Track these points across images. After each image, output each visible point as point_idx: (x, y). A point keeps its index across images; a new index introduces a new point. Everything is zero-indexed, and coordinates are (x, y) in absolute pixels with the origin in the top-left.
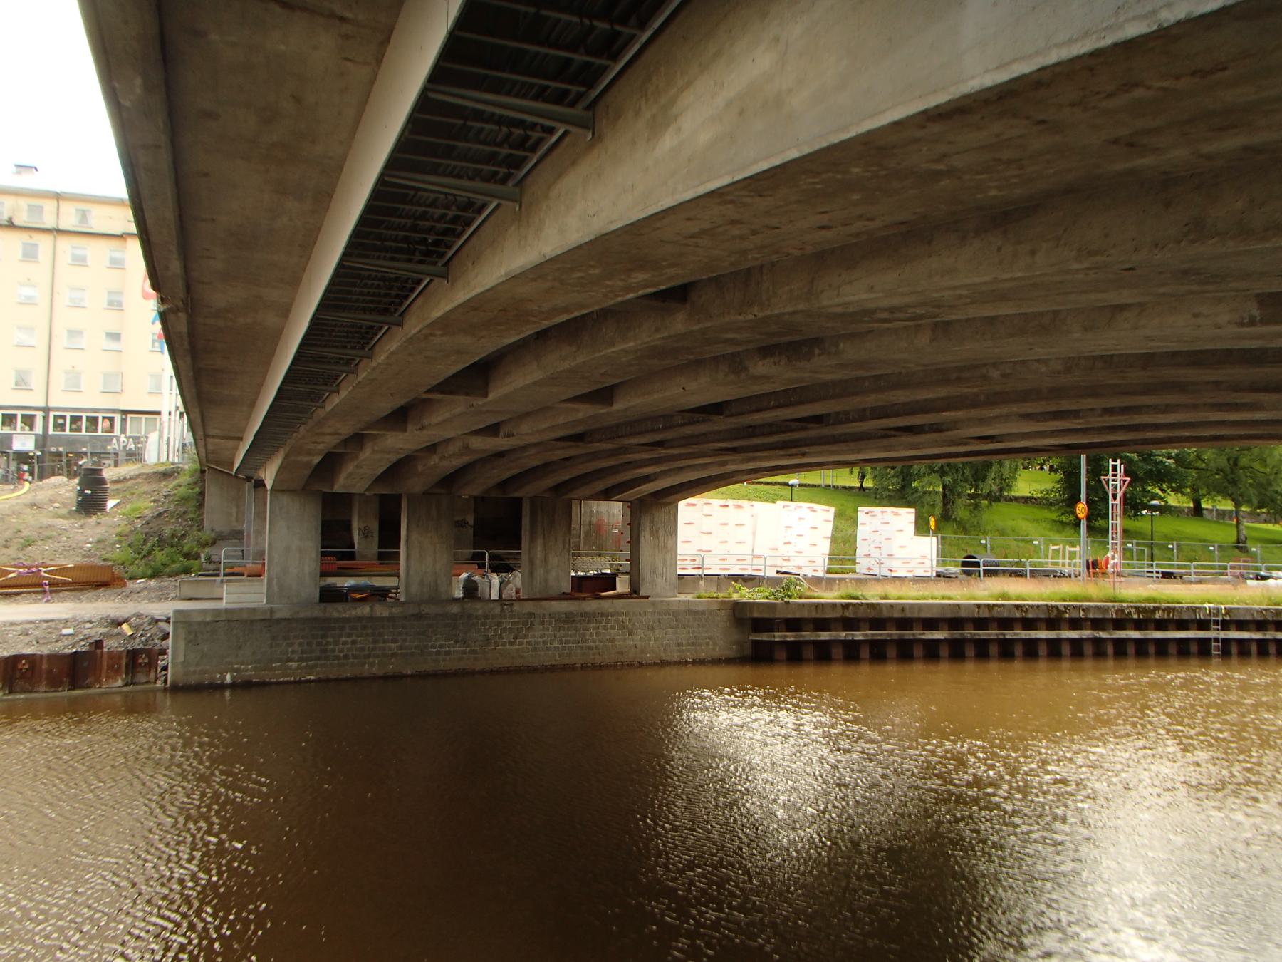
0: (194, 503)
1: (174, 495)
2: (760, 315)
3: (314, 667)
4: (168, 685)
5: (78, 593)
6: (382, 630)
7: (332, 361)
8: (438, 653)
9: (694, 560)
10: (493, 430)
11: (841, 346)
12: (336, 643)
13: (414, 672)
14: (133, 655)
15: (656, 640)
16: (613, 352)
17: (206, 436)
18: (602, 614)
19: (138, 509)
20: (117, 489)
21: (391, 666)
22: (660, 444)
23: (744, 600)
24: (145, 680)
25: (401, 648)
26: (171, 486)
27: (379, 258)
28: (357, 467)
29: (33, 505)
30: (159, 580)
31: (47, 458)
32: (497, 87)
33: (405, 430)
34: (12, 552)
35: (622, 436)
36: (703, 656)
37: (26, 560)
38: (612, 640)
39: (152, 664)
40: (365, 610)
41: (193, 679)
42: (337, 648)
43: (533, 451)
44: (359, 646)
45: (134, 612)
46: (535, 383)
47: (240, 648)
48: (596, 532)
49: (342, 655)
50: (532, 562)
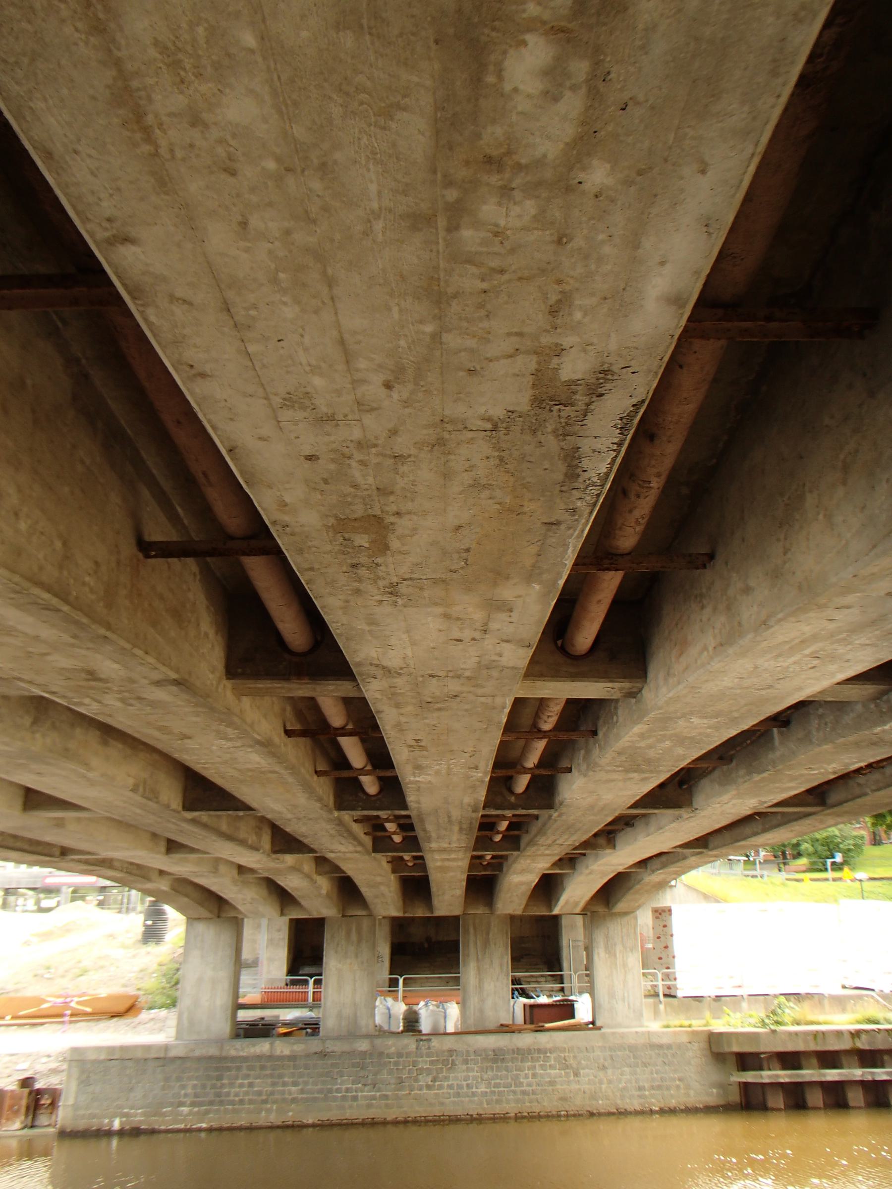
3: (207, 1112)
8: (344, 1098)
12: (231, 1085)
13: (316, 1121)
15: (610, 1082)
18: (539, 1051)
21: (291, 1114)
24: (46, 1123)
36: (673, 1103)
39: (53, 1105)
41: (82, 1125)
47: (132, 1090)
49: (237, 1099)
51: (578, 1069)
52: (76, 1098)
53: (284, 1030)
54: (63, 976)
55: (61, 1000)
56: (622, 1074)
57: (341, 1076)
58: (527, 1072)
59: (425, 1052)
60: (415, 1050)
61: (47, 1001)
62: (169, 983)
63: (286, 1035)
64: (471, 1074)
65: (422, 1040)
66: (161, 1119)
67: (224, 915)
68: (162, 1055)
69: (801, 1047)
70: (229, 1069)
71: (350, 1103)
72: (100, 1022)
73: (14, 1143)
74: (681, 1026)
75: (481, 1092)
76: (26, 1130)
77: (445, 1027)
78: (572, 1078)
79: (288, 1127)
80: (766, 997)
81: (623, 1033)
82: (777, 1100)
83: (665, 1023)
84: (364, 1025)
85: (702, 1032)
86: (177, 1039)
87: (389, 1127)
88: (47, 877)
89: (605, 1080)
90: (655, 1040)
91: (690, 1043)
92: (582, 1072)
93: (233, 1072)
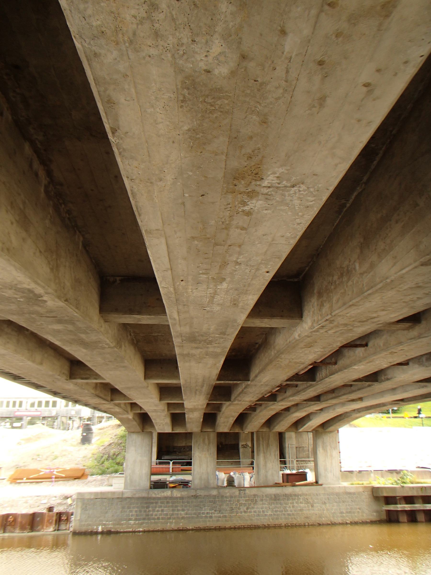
3: (142, 523)
8: (206, 517)
12: (154, 511)
14: (60, 515)
15: (327, 510)
18: (295, 495)
20: (100, 433)
21: (181, 524)
24: (64, 529)
36: (356, 519)
39: (68, 520)
41: (84, 529)
47: (107, 513)
49: (156, 517)
51: (313, 504)
52: (81, 516)
53: (172, 485)
54: (46, 460)
55: (48, 471)
56: (333, 506)
58: (290, 505)
59: (243, 496)
60: (238, 495)
61: (42, 471)
62: (99, 463)
63: (173, 487)
64: (264, 506)
65: (241, 490)
66: (121, 526)
67: (145, 430)
68: (121, 496)
69: (415, 494)
71: (209, 519)
72: (70, 481)
73: (50, 538)
74: (358, 484)
75: (269, 514)
76: (56, 531)
77: (244, 484)
78: (310, 508)
79: (180, 530)
80: (382, 471)
81: (333, 487)
82: (404, 518)
83: (351, 483)
84: (213, 482)
85: (369, 487)
86: (125, 489)
87: (227, 530)
88: (16, 412)
89: (325, 509)
90: (348, 491)
91: (363, 492)
92: (315, 505)
93: (154, 505)
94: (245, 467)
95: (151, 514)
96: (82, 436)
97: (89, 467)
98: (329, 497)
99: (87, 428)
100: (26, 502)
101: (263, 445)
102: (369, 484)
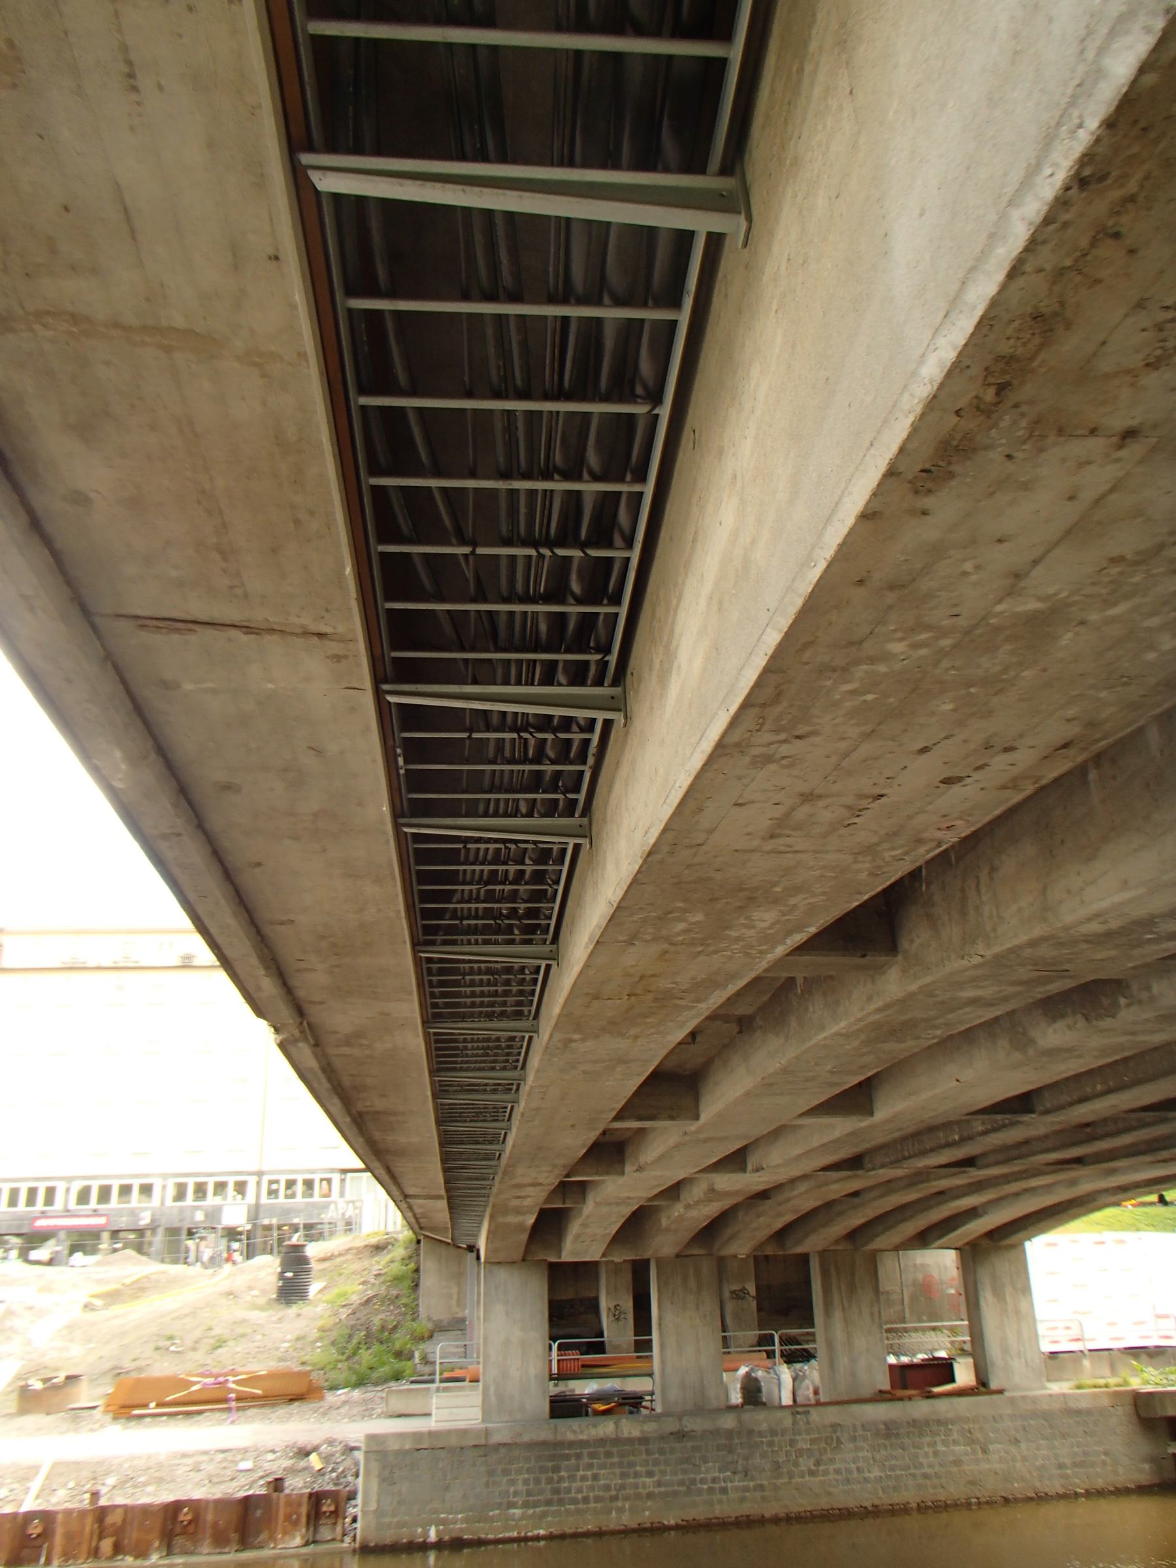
0: (408, 1283)
1: (385, 1273)
2: (989, 954)
3: (544, 1515)
4: (357, 1545)
5: (267, 1411)
6: (632, 1458)
7: (488, 1088)
8: (710, 1490)
9: (1068, 1328)
10: (736, 1160)
11: (1155, 989)
12: (572, 1478)
13: (680, 1522)
14: (316, 1498)
16: (826, 1038)
17: (406, 1196)
18: (939, 1422)
19: (345, 1294)
20: (324, 1269)
22: (969, 1162)
23: (1149, 1389)
24: (329, 1538)
25: (659, 1484)
26: (383, 1263)
27: (469, 943)
28: (584, 1225)
29: (230, 1294)
30: (363, 1389)
31: (259, 1232)
32: (481, 674)
33: (622, 1173)
34: (199, 1356)
35: (909, 1157)
36: (1100, 1483)
37: (215, 1367)
38: (957, 1463)
39: (337, 1514)
40: (606, 1428)
41: (388, 1537)
42: (574, 1485)
43: (803, 1187)
44: (602, 1482)
45: (324, 1438)
46: (747, 1094)
47: (447, 1488)
48: (925, 1290)
49: (580, 1496)
50: (830, 1345)
52: (378, 1501)
54: (194, 1349)
57: (705, 1462)
62: (343, 1354)
64: (860, 1454)
65: (798, 1413)
66: (487, 1525)
68: (483, 1442)
70: (567, 1457)
74: (1095, 1387)
78: (980, 1455)
79: (645, 1530)
85: (1126, 1392)
88: (36, 1218)
89: (1019, 1457)
90: (1073, 1405)
92: (991, 1447)
93: (573, 1461)
94: (742, 1352)
95: (565, 1488)
96: (280, 1279)
97: (317, 1367)
98: (1026, 1423)
99: (297, 1256)
100: (197, 1469)
101: (839, 1287)
102: (1121, 1386)
